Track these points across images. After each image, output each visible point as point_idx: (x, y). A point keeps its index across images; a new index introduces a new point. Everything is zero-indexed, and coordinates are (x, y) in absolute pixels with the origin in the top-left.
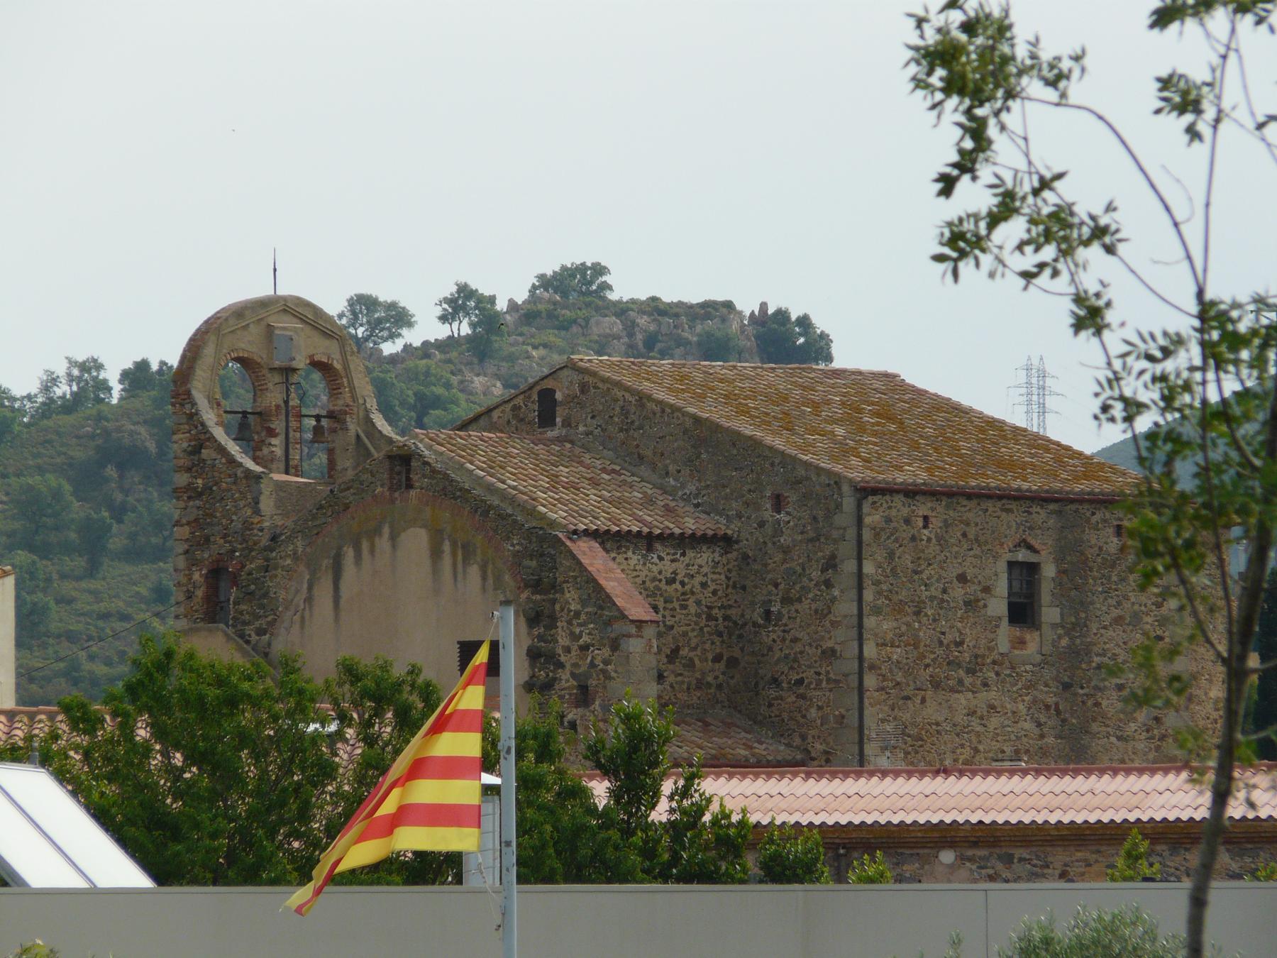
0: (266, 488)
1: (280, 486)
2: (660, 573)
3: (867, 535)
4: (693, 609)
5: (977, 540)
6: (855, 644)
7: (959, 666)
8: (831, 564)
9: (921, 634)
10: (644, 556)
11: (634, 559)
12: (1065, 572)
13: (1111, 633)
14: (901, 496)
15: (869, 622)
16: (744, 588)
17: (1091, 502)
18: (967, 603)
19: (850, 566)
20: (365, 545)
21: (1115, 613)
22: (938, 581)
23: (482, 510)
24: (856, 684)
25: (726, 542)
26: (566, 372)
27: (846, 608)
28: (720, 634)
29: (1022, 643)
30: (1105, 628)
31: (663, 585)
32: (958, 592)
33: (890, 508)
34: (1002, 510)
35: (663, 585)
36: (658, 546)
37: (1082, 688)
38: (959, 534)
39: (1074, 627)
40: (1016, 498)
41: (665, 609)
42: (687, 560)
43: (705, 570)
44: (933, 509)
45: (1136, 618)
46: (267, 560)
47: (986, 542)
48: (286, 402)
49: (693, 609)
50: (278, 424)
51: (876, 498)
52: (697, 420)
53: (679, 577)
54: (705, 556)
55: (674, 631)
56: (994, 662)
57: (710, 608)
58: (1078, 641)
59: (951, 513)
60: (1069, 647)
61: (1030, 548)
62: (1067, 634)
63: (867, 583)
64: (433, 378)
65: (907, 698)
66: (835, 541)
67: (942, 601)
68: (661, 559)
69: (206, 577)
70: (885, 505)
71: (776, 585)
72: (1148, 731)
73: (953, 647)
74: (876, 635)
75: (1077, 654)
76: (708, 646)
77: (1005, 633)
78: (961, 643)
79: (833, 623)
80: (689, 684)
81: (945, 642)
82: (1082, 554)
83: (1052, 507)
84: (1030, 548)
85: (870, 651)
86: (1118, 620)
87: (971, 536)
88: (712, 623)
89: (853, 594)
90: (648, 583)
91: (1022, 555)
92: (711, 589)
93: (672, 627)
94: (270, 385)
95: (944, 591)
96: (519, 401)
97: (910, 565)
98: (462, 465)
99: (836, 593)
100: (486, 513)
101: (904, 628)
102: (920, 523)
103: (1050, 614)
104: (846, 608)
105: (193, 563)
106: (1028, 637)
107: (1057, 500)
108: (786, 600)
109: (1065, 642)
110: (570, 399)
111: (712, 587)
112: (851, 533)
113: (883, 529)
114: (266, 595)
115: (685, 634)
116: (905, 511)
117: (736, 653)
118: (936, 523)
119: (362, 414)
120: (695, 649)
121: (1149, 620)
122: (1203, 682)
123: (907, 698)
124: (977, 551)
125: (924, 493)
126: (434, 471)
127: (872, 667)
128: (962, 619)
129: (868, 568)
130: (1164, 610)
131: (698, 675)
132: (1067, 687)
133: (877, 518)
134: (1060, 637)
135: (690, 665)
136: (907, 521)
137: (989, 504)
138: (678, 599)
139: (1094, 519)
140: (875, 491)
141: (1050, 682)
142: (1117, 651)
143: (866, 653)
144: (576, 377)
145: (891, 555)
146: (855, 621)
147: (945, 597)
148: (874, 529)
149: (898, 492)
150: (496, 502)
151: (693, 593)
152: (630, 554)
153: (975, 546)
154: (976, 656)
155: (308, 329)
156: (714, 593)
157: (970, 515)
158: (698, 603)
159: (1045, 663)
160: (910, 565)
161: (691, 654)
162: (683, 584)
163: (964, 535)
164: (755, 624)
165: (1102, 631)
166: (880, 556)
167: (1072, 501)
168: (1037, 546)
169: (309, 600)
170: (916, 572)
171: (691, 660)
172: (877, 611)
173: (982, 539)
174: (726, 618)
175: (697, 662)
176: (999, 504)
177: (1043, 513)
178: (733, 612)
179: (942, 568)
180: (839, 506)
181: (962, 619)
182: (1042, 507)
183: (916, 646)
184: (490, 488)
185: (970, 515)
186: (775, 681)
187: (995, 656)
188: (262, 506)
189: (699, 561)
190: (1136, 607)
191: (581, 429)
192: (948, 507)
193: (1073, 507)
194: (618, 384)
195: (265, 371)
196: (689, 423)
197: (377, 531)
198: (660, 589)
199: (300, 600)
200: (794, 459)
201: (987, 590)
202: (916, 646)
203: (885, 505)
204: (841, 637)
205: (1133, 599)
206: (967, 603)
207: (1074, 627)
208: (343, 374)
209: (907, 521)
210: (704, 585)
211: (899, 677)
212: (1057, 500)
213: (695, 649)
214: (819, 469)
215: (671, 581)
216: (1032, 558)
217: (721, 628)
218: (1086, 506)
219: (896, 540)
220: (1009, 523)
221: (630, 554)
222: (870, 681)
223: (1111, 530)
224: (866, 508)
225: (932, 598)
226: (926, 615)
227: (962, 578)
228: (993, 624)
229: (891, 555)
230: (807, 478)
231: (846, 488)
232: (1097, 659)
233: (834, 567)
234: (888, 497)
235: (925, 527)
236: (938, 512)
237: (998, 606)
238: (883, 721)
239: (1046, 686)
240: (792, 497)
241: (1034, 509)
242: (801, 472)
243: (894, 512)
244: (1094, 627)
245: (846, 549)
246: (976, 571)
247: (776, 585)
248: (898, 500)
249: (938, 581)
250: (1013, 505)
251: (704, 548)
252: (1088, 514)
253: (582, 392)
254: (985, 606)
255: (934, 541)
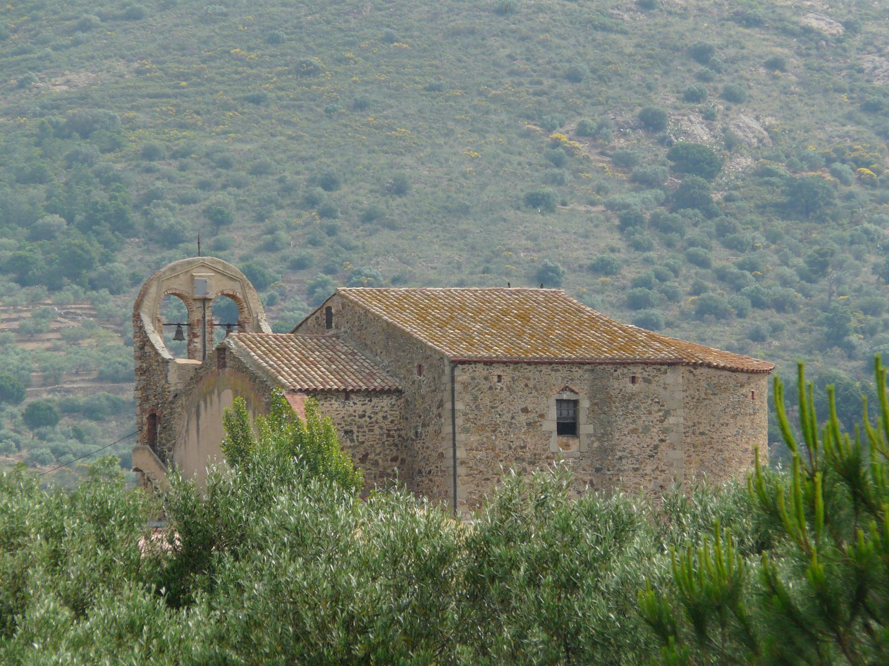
0: (171, 367)
1: (181, 367)
2: (355, 411)
3: (458, 387)
4: (377, 431)
5: (535, 387)
6: (451, 450)
7: (523, 460)
8: (441, 405)
9: (497, 443)
10: (344, 403)
11: (336, 405)
12: (596, 404)
13: (628, 438)
14: (482, 365)
15: (461, 437)
16: (407, 419)
17: (614, 364)
18: (529, 424)
19: (448, 406)
20: (208, 400)
21: (631, 427)
22: (508, 412)
23: (254, 378)
24: (452, 473)
25: (399, 392)
26: (335, 297)
27: (448, 429)
28: (396, 445)
29: (567, 446)
30: (625, 435)
31: (357, 419)
32: (522, 418)
33: (474, 371)
34: (552, 370)
35: (357, 419)
36: (353, 396)
37: (609, 470)
38: (523, 385)
39: (603, 436)
40: (561, 363)
41: (358, 432)
42: (373, 404)
43: (386, 409)
44: (504, 371)
45: (646, 430)
46: (171, 409)
47: (541, 389)
48: (204, 318)
49: (377, 431)
50: (198, 330)
51: (464, 366)
52: (388, 324)
53: (367, 414)
54: (385, 401)
55: (365, 445)
56: (548, 458)
57: (389, 430)
58: (606, 444)
59: (517, 373)
60: (599, 447)
61: (572, 391)
62: (599, 439)
63: (457, 414)
64: (847, 286)
65: (488, 479)
66: (442, 391)
67: (511, 423)
68: (355, 404)
69: (148, 418)
70: (471, 370)
71: (420, 417)
72: (655, 494)
73: (519, 450)
74: (466, 445)
75: (604, 452)
76: (387, 452)
77: (555, 443)
78: (525, 447)
79: (442, 438)
80: (375, 474)
81: (513, 447)
82: (608, 393)
83: (586, 367)
84: (572, 391)
85: (461, 454)
86: (634, 431)
87: (531, 386)
88: (391, 439)
89: (450, 421)
90: (346, 418)
91: (566, 396)
92: (390, 420)
93: (363, 443)
94: (194, 308)
95: (513, 418)
96: (318, 314)
97: (489, 404)
98: (249, 353)
99: (443, 420)
100: (254, 381)
101: (485, 440)
102: (496, 379)
103: (585, 428)
104: (448, 429)
105: (143, 411)
106: (571, 442)
107: (589, 363)
108: (424, 425)
109: (596, 445)
110: (338, 312)
111: (390, 418)
112: (449, 386)
113: (469, 384)
114: (171, 429)
115: (372, 446)
116: (485, 373)
117: (404, 456)
118: (506, 379)
119: (255, 323)
120: (379, 454)
121: (655, 430)
122: (734, 463)
123: (488, 479)
124: (535, 393)
125: (498, 362)
126: (234, 357)
127: (462, 463)
128: (525, 433)
129: (459, 406)
130: (665, 424)
131: (381, 469)
132: (598, 470)
133: (465, 377)
134: (593, 442)
135: (376, 463)
136: (486, 379)
137: (543, 368)
138: (367, 426)
139: (616, 374)
140: (463, 362)
141: (587, 468)
142: (633, 448)
143: (458, 455)
144: (340, 300)
145: (475, 399)
146: (451, 436)
147: (513, 421)
148: (463, 384)
149: (479, 362)
150: (260, 374)
151: (377, 422)
152: (333, 401)
153: (534, 391)
154: (535, 455)
155: (219, 276)
156: (392, 422)
157: (530, 374)
158: (381, 428)
159: (582, 457)
160: (489, 404)
161: (377, 458)
162: (370, 418)
163: (526, 385)
164: (412, 440)
165: (624, 437)
166: (468, 398)
167: (601, 364)
168: (576, 390)
169: (187, 431)
170: (492, 408)
171: (376, 461)
172: (466, 431)
173: (538, 387)
174: (399, 436)
175: (380, 461)
176: (550, 367)
177: (581, 372)
178: (403, 433)
179: (511, 405)
180: (443, 371)
181: (525, 433)
182: (580, 368)
183: (493, 450)
184: (259, 367)
185: (530, 374)
186: (420, 472)
187: (548, 453)
188: (169, 378)
189: (382, 404)
190: (646, 423)
191: (343, 329)
192: (514, 370)
193: (602, 367)
194: (356, 303)
195: (191, 301)
196: (385, 325)
197: (212, 392)
198: (354, 421)
199: (184, 431)
200: (425, 344)
201: (542, 416)
202: (493, 450)
203: (471, 370)
204: (445, 447)
205: (644, 419)
206: (529, 424)
207: (603, 436)
208: (243, 300)
209: (486, 379)
210: (385, 418)
211: (482, 467)
212: (589, 363)
213: (379, 454)
214: (436, 350)
215: (363, 416)
216: (572, 397)
217: (396, 441)
218: (610, 366)
219: (479, 390)
220: (557, 378)
221: (333, 401)
222: (461, 470)
223: (627, 380)
224: (457, 372)
225: (504, 422)
226: (500, 432)
227: (525, 410)
228: (547, 436)
229: (475, 399)
230: (431, 356)
231: (446, 362)
232: (619, 454)
233: (442, 406)
234: (473, 365)
235: (499, 381)
236: (508, 374)
237: (550, 424)
238: (470, 493)
239: (584, 470)
240: (425, 366)
241: (574, 369)
242: (429, 353)
243: (477, 374)
244: (617, 435)
245: (447, 395)
246: (534, 405)
247: (420, 417)
248: (480, 366)
249: (508, 412)
250: (560, 367)
251: (385, 397)
252: (612, 371)
253: (343, 308)
254: (541, 425)
255: (505, 389)
